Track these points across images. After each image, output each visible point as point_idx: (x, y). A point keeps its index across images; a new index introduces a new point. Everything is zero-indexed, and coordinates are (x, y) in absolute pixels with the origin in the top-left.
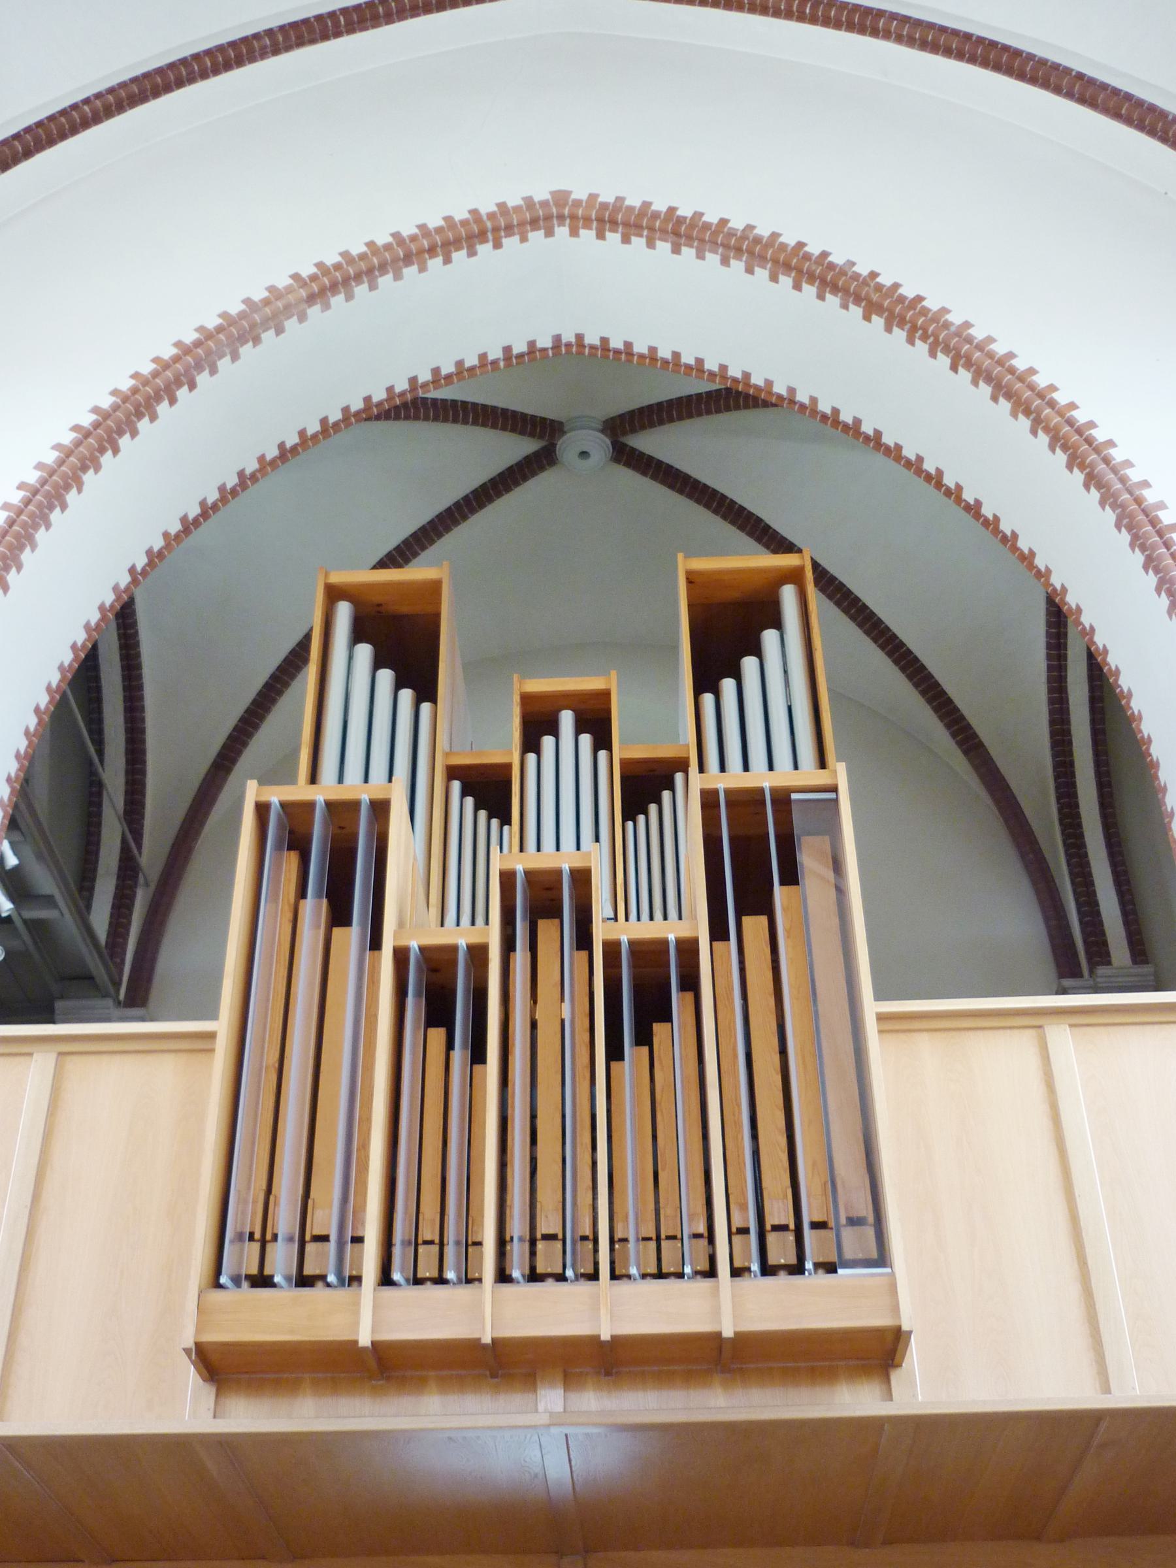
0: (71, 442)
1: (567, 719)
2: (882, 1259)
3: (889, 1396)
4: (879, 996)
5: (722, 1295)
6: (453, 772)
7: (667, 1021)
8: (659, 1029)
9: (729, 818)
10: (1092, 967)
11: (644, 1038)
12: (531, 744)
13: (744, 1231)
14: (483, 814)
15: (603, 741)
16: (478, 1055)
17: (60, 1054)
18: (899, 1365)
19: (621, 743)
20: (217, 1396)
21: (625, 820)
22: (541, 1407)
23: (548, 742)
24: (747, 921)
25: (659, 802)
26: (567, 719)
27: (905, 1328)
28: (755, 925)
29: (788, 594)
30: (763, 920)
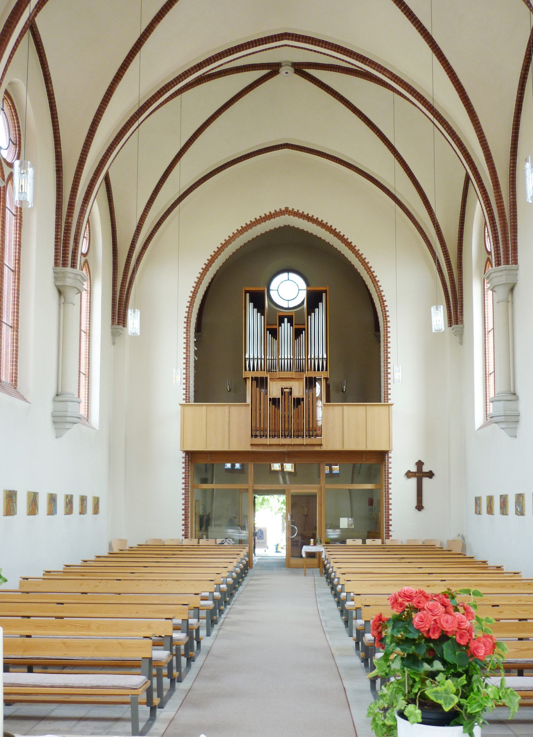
1: (286, 320)
11: (297, 407)
12: (280, 325)
23: (283, 324)
26: (286, 320)
29: (324, 294)
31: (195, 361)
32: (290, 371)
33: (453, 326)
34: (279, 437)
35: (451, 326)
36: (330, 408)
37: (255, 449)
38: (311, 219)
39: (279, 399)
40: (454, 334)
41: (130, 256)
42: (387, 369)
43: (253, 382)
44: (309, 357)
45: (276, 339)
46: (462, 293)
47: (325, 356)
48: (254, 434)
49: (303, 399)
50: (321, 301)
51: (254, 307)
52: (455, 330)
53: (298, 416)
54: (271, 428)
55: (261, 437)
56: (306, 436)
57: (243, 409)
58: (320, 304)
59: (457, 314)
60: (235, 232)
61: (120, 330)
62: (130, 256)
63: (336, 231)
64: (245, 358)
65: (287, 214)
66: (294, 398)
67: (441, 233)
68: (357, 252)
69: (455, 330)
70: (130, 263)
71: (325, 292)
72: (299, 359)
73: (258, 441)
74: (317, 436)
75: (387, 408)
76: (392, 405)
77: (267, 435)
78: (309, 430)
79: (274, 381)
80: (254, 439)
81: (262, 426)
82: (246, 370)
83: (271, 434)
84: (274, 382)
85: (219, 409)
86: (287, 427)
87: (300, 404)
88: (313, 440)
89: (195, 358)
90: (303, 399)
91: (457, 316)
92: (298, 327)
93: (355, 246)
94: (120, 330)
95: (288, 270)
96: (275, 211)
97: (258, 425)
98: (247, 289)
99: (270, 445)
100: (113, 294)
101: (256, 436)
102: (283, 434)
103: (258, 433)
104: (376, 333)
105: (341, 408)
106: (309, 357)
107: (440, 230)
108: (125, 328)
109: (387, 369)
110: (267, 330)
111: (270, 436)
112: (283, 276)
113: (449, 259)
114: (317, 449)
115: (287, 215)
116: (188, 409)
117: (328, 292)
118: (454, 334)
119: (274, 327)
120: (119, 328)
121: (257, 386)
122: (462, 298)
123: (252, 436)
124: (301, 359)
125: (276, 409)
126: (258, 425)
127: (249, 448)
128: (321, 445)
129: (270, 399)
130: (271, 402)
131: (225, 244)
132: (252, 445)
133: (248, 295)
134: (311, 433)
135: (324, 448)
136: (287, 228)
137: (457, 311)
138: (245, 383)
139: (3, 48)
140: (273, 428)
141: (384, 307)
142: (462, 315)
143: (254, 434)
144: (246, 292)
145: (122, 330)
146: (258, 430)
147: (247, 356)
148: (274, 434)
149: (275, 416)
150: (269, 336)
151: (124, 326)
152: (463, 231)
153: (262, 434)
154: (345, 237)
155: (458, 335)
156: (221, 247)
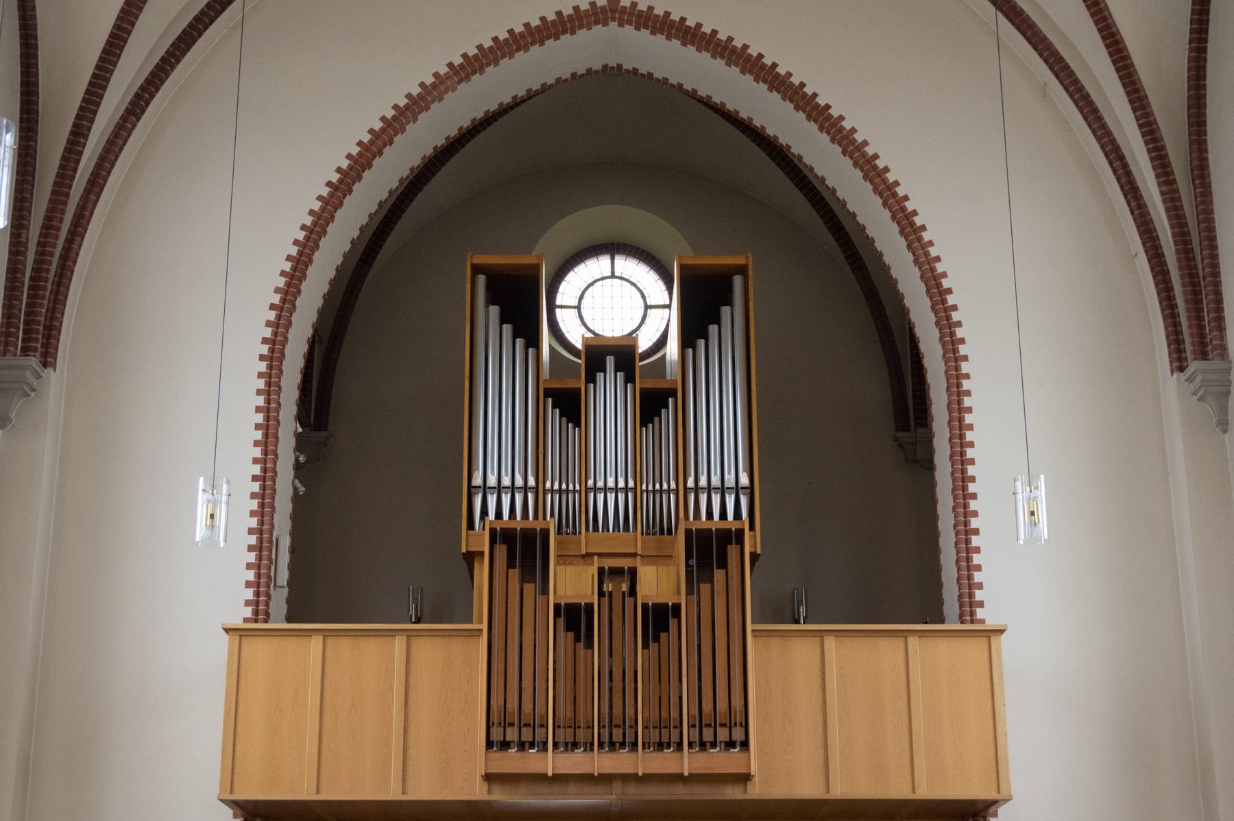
0: (328, 194)
1: (610, 361)
2: (745, 744)
3: (745, 792)
4: (753, 622)
5: (684, 757)
6: (549, 393)
7: (666, 632)
8: (663, 635)
9: (696, 553)
10: (917, 425)
11: (657, 639)
12: (591, 379)
13: (694, 726)
14: (564, 419)
15: (630, 379)
16: (589, 645)
17: (408, 636)
18: (751, 780)
19: (641, 377)
20: (488, 786)
21: (641, 427)
22: (614, 792)
23: (600, 376)
24: (702, 585)
25: (660, 416)
26: (610, 361)
27: (752, 773)
28: (705, 588)
29: (737, 280)
30: (709, 586)
31: (296, 498)
32: (626, 528)
33: (1194, 366)
34: (589, 747)
35: (1181, 369)
36: (775, 642)
37: (502, 796)
38: (694, 35)
39: (589, 607)
40: (1194, 394)
41: (79, 132)
42: (965, 516)
43: (497, 546)
44: (691, 483)
45: (577, 424)
46: (1214, 257)
47: (744, 480)
48: (497, 735)
49: (677, 608)
50: (729, 302)
51: (503, 321)
52: (1199, 378)
53: (662, 674)
54: (561, 715)
55: (522, 746)
56: (690, 745)
57: (458, 647)
58: (725, 311)
59: (1201, 327)
60: (443, 70)
61: (28, 374)
62: (79, 132)
63: (778, 70)
64: (470, 486)
65: (613, 19)
66: (645, 606)
67: (1132, 65)
68: (847, 137)
69: (1199, 378)
70: (80, 153)
71: (742, 270)
72: (654, 491)
73: (512, 762)
74: (730, 744)
75: (981, 643)
76: (1001, 631)
77: (545, 743)
78: (699, 724)
79: (571, 564)
80: (496, 755)
81: (527, 707)
82: (471, 526)
83: (561, 740)
84: (569, 568)
85: (371, 649)
86: (617, 710)
87: (667, 630)
88: (719, 761)
89: (295, 489)
90: (677, 608)
91: (1201, 335)
92: (650, 384)
93: (841, 118)
94: (28, 374)
95: (613, 248)
96: (576, 8)
97: (513, 705)
98: (481, 259)
99: (559, 779)
100: (11, 252)
101: (505, 745)
102: (607, 740)
103: (512, 734)
104: (899, 434)
105: (813, 643)
106: (691, 483)
107: (1128, 57)
108: (50, 370)
109: (965, 516)
110: (546, 395)
111: (555, 745)
112: (597, 266)
113: (1163, 148)
114: (733, 793)
115: (613, 25)
116: (258, 649)
117: (751, 273)
118: (1194, 394)
119: (571, 384)
120: (25, 368)
121: (511, 565)
122: (1216, 274)
123: (489, 744)
124: (661, 491)
125: (581, 645)
126: (513, 705)
127: (477, 791)
128: (745, 778)
129: (557, 607)
130: (561, 621)
131: (407, 107)
132: (489, 778)
133: (481, 279)
134: (708, 735)
135: (756, 791)
136: (614, 74)
137: (1200, 319)
138: (470, 584)
139: (78, 211)
140: (570, 715)
141: (946, 310)
142: (1221, 329)
143: (497, 735)
144: (477, 270)
145: (39, 377)
146: (512, 724)
147: (478, 480)
148: (570, 739)
149: (573, 676)
150: (553, 415)
151: (45, 365)
152: (1205, 60)
153: (527, 735)
154: (805, 90)
155: (1210, 398)
156: (395, 118)
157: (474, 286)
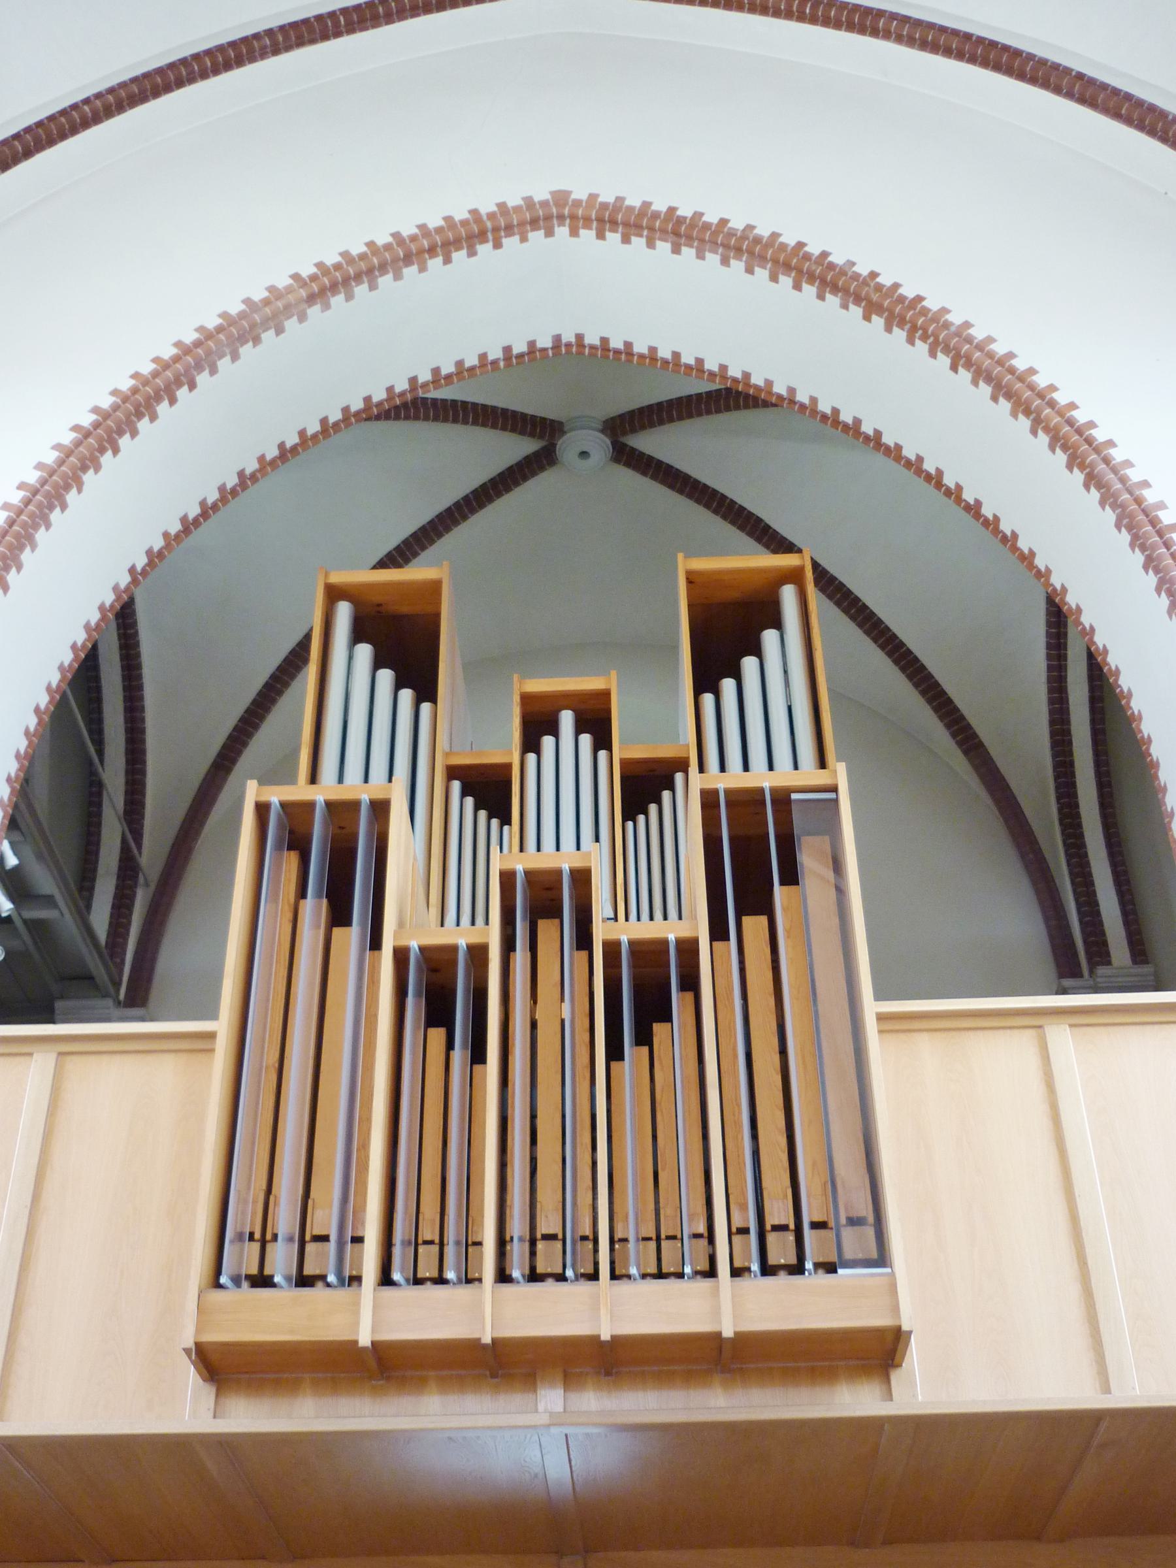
0: (71, 442)
1: (567, 719)
2: (882, 1259)
3: (889, 1396)
4: (879, 996)
5: (722, 1295)
6: (453, 772)
7: (667, 1021)
8: (659, 1029)
9: (729, 818)
10: (1092, 967)
11: (644, 1038)
12: (531, 744)
13: (744, 1231)
14: (483, 814)
15: (603, 741)
16: (478, 1055)
17: (60, 1054)
18: (899, 1365)
19: (621, 743)
20: (217, 1396)
21: (625, 820)
22: (541, 1407)
23: (548, 742)
24: (747, 921)
25: (659, 802)
26: (567, 719)
27: (905, 1328)
28: (755, 925)
29: (788, 594)
30: (763, 920)
157: (504, 1147)
